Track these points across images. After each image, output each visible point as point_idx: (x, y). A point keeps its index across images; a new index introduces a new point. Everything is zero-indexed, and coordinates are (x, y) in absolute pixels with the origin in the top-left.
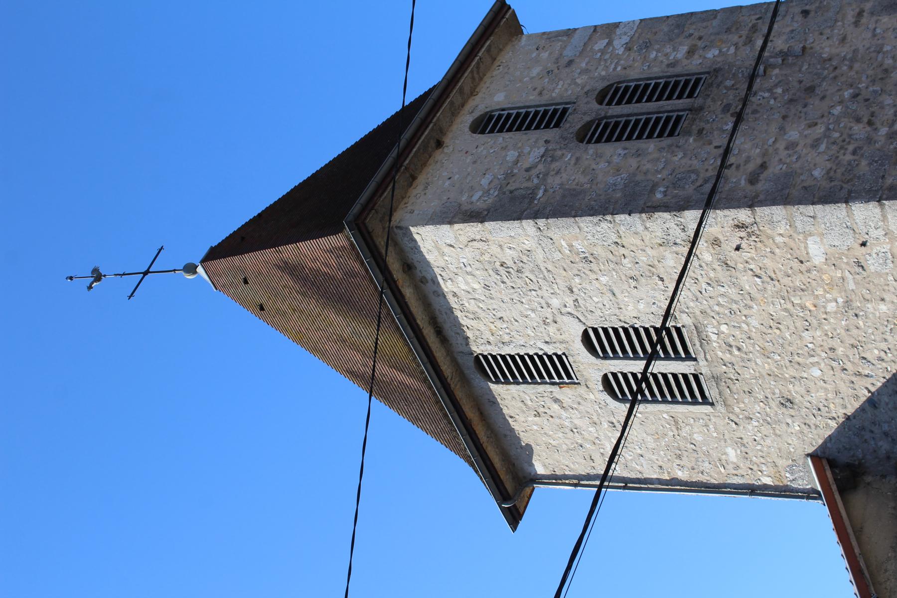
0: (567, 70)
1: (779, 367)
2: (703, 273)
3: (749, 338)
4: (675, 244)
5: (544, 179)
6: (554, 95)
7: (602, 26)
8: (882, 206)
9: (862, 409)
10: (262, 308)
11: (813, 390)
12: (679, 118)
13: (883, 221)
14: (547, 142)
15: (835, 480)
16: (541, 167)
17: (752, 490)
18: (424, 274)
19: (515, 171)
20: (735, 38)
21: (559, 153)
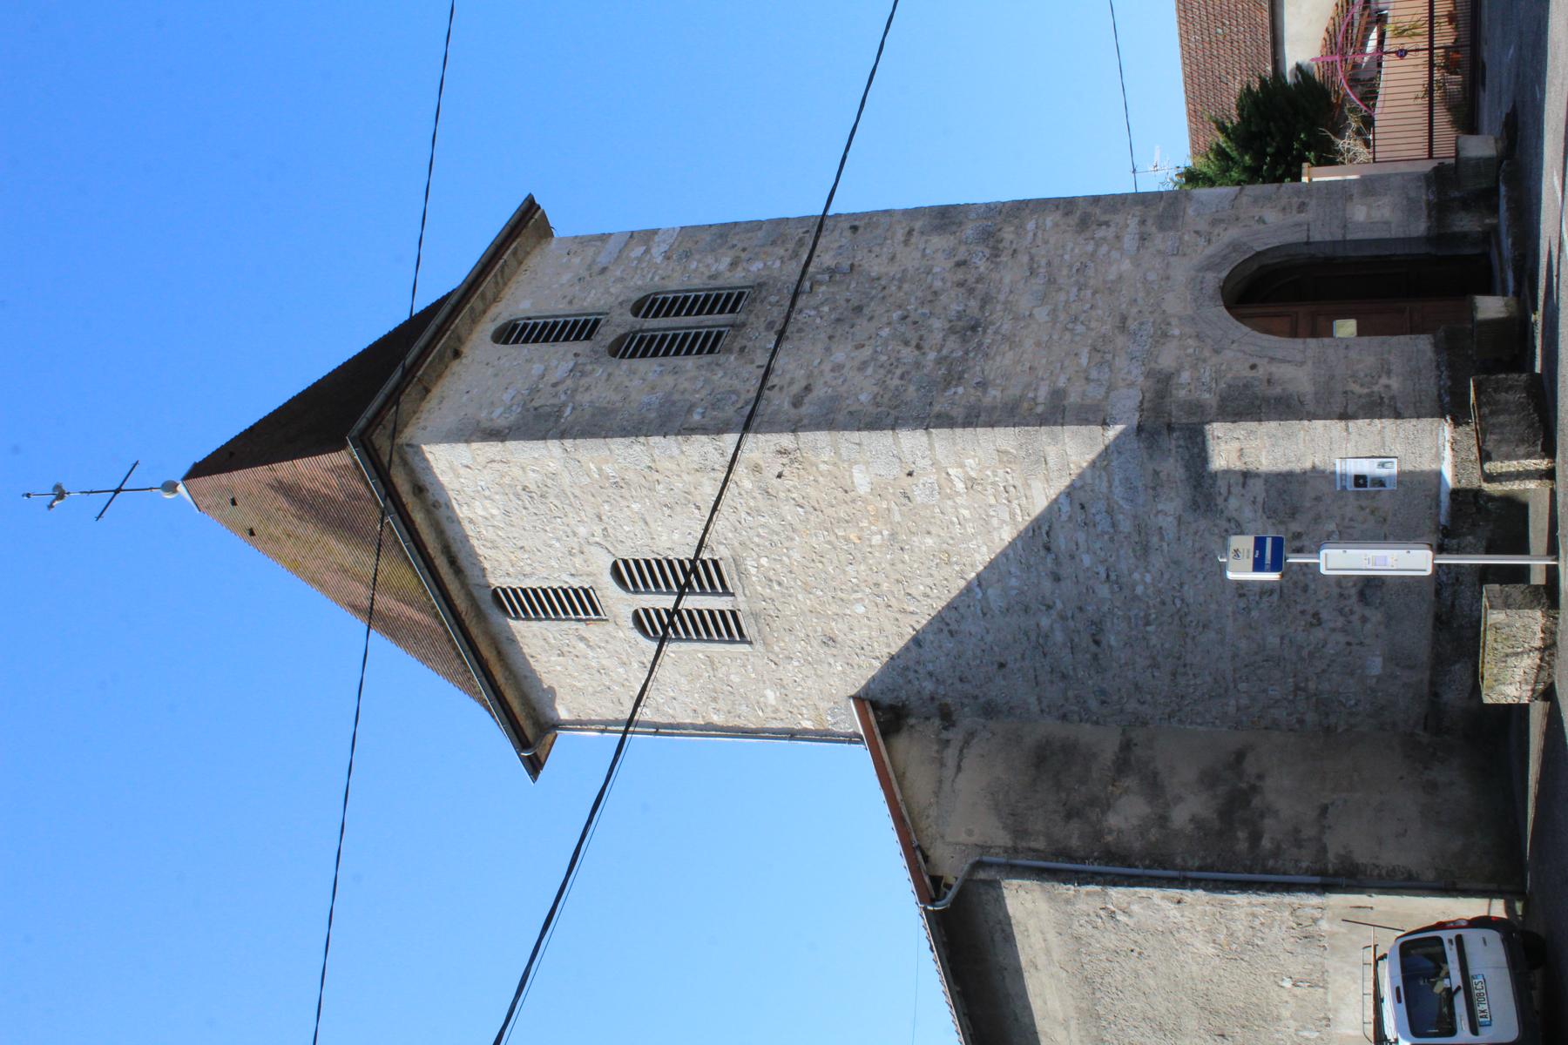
1: (822, 603)
3: (791, 572)
5: (572, 396)
6: (585, 304)
8: (929, 434)
9: (906, 648)
10: (252, 533)
12: (719, 335)
14: (576, 355)
15: (878, 722)
16: (569, 382)
17: (792, 735)
18: (437, 497)
19: (541, 386)
21: (589, 367)
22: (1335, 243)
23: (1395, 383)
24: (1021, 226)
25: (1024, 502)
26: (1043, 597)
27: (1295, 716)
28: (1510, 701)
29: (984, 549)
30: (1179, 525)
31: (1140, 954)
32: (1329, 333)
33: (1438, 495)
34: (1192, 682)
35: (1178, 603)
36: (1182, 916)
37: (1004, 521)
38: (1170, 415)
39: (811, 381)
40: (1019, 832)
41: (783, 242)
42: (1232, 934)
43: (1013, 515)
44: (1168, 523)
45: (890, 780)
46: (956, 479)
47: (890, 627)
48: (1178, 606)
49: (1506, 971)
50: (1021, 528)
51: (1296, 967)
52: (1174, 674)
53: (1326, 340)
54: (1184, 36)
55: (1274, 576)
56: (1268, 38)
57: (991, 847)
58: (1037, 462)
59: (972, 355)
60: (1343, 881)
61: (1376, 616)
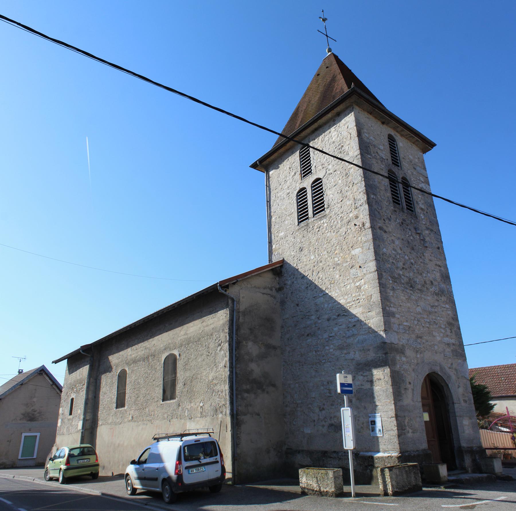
0: (412, 168)
1: (313, 245)
2: (345, 214)
3: (323, 234)
4: (355, 203)
5: (374, 158)
6: (404, 163)
7: (428, 180)
8: (375, 271)
9: (301, 274)
10: (318, 75)
11: (306, 257)
12: (399, 204)
13: (369, 272)
14: (387, 159)
15: (276, 267)
16: (378, 157)
17: (270, 242)
18: (336, 120)
19: (376, 148)
20: (428, 224)
21: (384, 163)
22: (455, 412)
23: (410, 435)
24: (447, 303)
25: (354, 306)
26: (322, 316)
27: (288, 404)
28: (300, 479)
29: (336, 295)
30: (351, 359)
31: (208, 355)
32: (424, 411)
33: (370, 451)
34: (297, 368)
35: (324, 361)
36: (221, 368)
37: (347, 300)
38: (391, 353)
39: (388, 233)
40: (244, 313)
41: (431, 225)
42: (216, 385)
43: (349, 303)
44: (351, 355)
45: (258, 271)
46: (360, 283)
47: (307, 268)
48: (323, 361)
49: (207, 479)
50: (345, 306)
51: (207, 407)
52: (299, 362)
53: (422, 410)
54: (499, 367)
55: (339, 391)
56: (503, 395)
57: (239, 304)
58: (369, 309)
59: (403, 286)
60: (235, 421)
61: (325, 430)
